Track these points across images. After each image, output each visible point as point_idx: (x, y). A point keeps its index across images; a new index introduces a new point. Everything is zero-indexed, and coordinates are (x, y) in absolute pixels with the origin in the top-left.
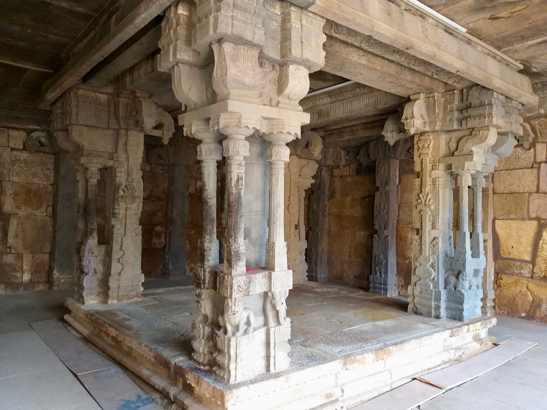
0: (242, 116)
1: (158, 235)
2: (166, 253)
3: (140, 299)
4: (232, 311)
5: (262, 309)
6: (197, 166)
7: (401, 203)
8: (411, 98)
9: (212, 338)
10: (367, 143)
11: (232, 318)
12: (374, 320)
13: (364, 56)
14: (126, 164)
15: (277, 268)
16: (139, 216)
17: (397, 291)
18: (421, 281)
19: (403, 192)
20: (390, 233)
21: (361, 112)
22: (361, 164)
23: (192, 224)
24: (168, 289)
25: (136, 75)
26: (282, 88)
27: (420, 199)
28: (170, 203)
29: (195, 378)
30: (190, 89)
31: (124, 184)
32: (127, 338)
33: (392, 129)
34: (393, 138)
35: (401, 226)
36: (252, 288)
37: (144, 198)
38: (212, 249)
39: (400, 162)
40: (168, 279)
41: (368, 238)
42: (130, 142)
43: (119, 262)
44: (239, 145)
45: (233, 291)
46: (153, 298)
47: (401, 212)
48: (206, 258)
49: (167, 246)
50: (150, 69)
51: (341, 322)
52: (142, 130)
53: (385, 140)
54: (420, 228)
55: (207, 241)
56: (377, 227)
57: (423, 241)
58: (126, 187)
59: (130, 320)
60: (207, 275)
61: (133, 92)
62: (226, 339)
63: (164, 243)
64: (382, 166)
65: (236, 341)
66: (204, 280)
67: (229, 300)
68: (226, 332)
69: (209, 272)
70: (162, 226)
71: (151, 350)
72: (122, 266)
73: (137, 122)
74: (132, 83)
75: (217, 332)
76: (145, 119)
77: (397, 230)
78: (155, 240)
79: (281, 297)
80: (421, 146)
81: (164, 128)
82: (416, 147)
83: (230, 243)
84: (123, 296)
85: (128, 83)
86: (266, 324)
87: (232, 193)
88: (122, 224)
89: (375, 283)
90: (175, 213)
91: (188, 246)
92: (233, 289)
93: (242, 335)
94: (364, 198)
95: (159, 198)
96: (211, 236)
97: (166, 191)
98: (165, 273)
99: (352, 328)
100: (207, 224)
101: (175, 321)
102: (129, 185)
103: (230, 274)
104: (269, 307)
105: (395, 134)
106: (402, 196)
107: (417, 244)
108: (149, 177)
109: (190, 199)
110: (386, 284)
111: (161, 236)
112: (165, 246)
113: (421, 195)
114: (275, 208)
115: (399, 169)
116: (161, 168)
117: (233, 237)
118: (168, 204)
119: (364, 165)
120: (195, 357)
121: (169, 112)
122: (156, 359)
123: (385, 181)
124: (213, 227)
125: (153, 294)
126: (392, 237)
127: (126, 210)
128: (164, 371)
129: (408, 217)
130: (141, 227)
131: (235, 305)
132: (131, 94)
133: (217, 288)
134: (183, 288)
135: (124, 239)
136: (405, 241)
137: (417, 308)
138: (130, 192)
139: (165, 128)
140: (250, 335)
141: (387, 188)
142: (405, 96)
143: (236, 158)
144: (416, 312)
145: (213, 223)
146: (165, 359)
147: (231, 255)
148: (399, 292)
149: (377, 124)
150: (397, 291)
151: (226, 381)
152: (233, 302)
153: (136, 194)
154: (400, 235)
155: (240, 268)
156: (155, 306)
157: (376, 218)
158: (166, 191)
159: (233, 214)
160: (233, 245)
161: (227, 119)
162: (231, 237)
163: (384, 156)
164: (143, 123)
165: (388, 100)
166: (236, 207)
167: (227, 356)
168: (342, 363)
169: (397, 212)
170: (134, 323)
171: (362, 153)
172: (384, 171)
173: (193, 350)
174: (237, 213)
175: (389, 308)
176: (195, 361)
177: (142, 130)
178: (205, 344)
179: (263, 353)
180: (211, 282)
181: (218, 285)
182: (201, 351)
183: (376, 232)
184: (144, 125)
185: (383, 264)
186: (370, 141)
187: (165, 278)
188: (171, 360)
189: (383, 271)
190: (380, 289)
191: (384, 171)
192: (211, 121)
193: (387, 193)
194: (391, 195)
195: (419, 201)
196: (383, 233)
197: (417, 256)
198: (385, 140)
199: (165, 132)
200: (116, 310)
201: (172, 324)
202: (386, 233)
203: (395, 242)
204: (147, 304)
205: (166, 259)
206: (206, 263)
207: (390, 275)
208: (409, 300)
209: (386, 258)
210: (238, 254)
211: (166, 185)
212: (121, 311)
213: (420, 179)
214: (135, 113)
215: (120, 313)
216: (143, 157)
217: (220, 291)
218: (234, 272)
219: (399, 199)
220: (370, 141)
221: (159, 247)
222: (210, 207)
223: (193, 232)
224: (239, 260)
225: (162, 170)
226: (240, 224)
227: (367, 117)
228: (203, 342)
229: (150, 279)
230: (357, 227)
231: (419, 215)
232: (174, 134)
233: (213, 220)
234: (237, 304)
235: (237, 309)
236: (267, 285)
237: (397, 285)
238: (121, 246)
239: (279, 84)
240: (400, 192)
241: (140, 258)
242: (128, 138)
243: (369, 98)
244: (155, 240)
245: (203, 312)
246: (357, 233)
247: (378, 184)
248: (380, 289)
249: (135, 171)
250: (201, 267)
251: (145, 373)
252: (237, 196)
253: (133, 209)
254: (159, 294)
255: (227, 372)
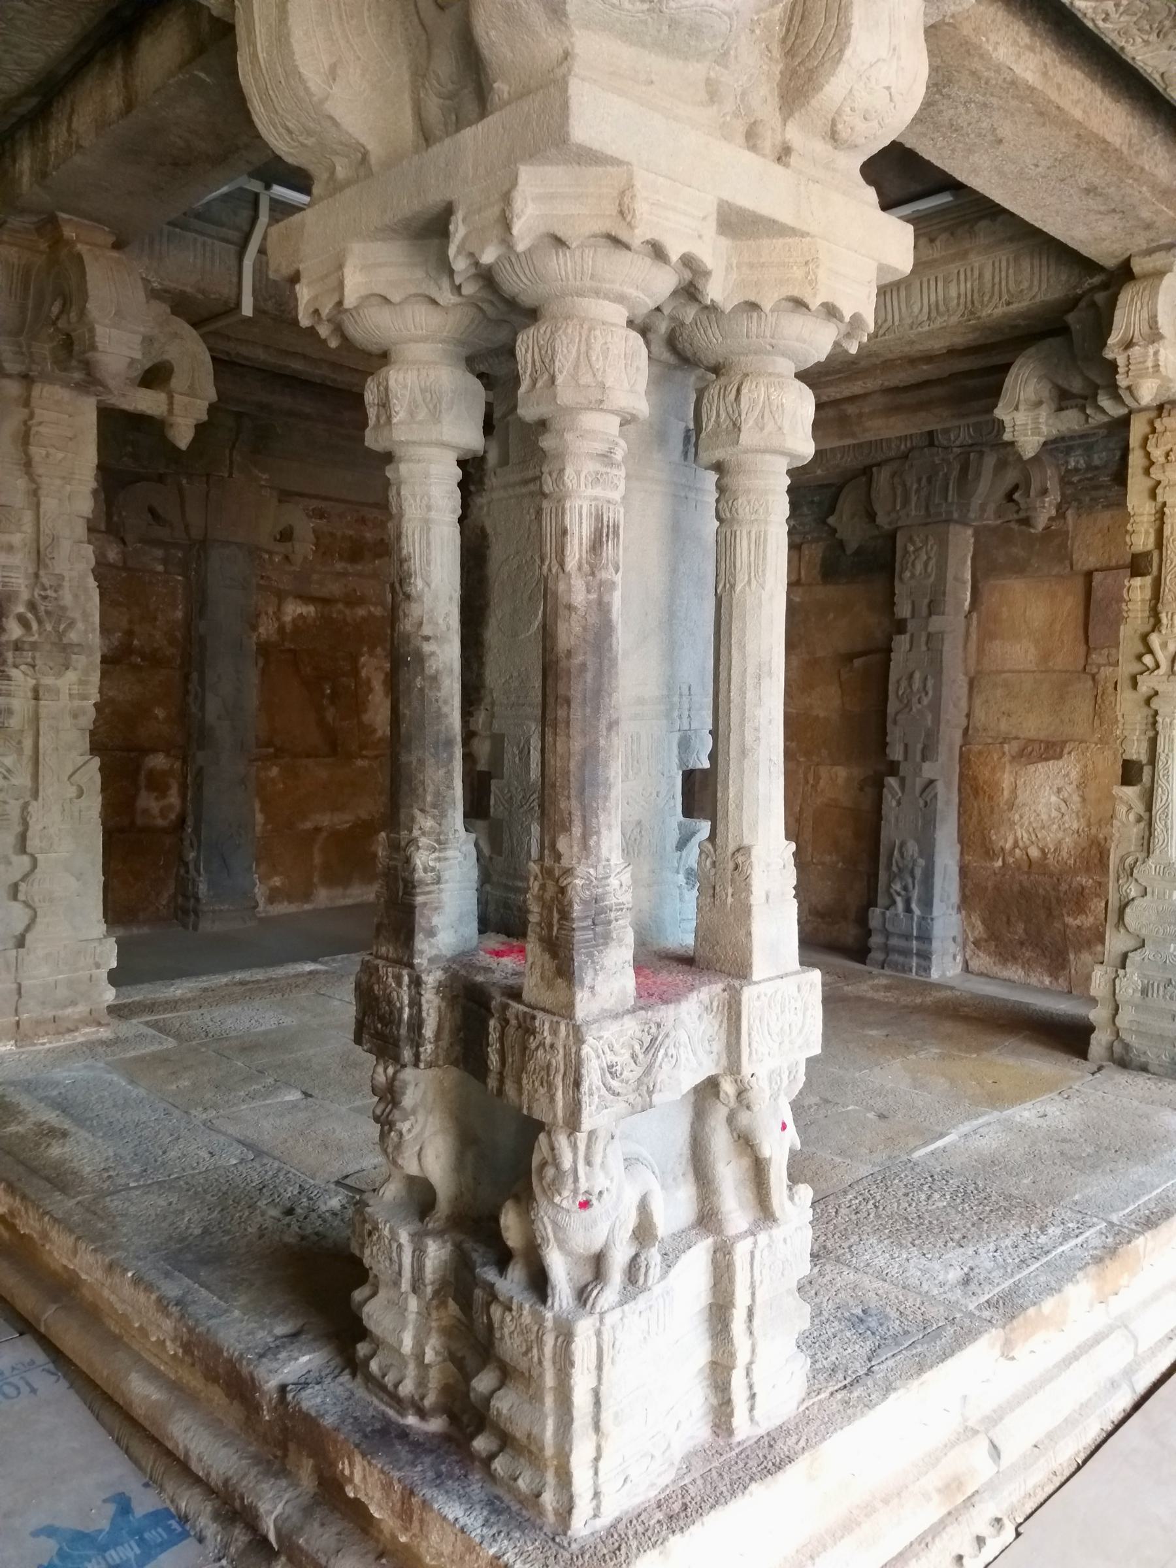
0: (638, 184)
1: (157, 784)
2: (187, 843)
3: (104, 1033)
4: (575, 1192)
5: (686, 1151)
6: (280, 548)
7: (978, 672)
8: (1137, 266)
9: (462, 1292)
10: (867, 471)
11: (575, 1221)
12: (996, 1100)
13: (1031, 49)
14: (28, 517)
15: (759, 969)
16: (89, 717)
17: (959, 958)
18: (1148, 951)
19: (987, 635)
20: (942, 770)
21: (912, 334)
22: (841, 545)
23: (269, 744)
24: (205, 982)
25: (57, 138)
26: (811, 71)
27: (1150, 651)
28: (195, 676)
29: (387, 1487)
30: (333, 69)
31: (25, 595)
32: (54, 1234)
33: (1033, 397)
34: (1036, 431)
35: (976, 748)
36: (663, 1074)
37: (104, 660)
38: (446, 875)
39: (976, 534)
40: (195, 928)
41: (861, 789)
42: (41, 429)
43: (15, 897)
44: (606, 352)
45: (585, 1099)
46: (154, 1025)
47: (978, 702)
48: (420, 921)
49: (190, 821)
50: (116, 103)
51: (882, 1116)
52: (90, 380)
53: (1007, 437)
54: (1144, 758)
55: (423, 841)
56: (896, 753)
57: (1158, 806)
58: (32, 606)
59: (65, 1134)
60: (431, 1002)
61: (49, 225)
62: (549, 1324)
63: (178, 809)
64: (917, 550)
65: (599, 1334)
66: (417, 1024)
67: (562, 1141)
68: (539, 1283)
69: (440, 988)
70: (168, 755)
71: (162, 1305)
72: (29, 912)
73: (68, 343)
74: (41, 175)
75: (489, 1274)
76: (99, 330)
77: (964, 760)
78: (147, 802)
79: (775, 1097)
80: (1157, 454)
81: (174, 383)
82: (1136, 460)
83: (558, 857)
84: (38, 1023)
85: (25, 180)
86: (707, 1218)
87: (569, 607)
88: (20, 751)
89: (887, 935)
90: (213, 707)
91: (260, 818)
92: (585, 1087)
93: (622, 1303)
94: (850, 657)
95: (154, 660)
96: (443, 815)
97: (178, 634)
98: (185, 910)
99: (940, 1143)
100: (421, 762)
101: (251, 1134)
102: (45, 598)
103: (567, 1010)
104: (720, 1141)
105: (1044, 413)
106: (981, 651)
107: (1132, 817)
108: (118, 585)
109: (261, 663)
110: (925, 937)
111: (168, 787)
112: (182, 821)
113: (1155, 640)
114: (750, 682)
115: (974, 559)
116: (159, 553)
117: (577, 831)
118: (186, 678)
119: (852, 546)
120: (374, 1366)
121: (195, 325)
122: (187, 1347)
123: (926, 601)
124: (449, 773)
125: (151, 1007)
126: (948, 785)
127: (37, 698)
128: (233, 1413)
129: (1004, 720)
130: (96, 762)
131: (589, 1163)
132: (39, 229)
133: (486, 1069)
134: (259, 975)
135: (34, 807)
136: (991, 798)
137: (1127, 1047)
138: (49, 627)
139: (178, 382)
140: (657, 1290)
141: (936, 624)
142: (1102, 262)
143: (591, 420)
144: (1124, 1060)
145: (451, 758)
146: (230, 1361)
147: (565, 915)
148: (966, 963)
149: (937, 391)
150: (959, 958)
151: (551, 1518)
152: (582, 1146)
153: (73, 636)
154: (975, 778)
155: (608, 979)
156: (161, 1059)
157: (895, 722)
158: (178, 634)
159: (576, 713)
160: (581, 870)
161: (552, 197)
162: (566, 828)
163: (928, 514)
164: (93, 347)
165: (1025, 285)
166: (589, 676)
167: (549, 1401)
168: (998, 1345)
169: (964, 704)
170: (82, 1152)
171: (847, 505)
172: (926, 564)
173: (363, 1333)
174: (597, 710)
175: (1012, 1042)
176: (376, 1384)
177: (90, 380)
178: (425, 1313)
179: (700, 1352)
180: (446, 1035)
181: (494, 1059)
182: (407, 1344)
183: (893, 768)
184: (98, 356)
185: (918, 872)
186: (879, 465)
187: (185, 926)
188: (261, 1372)
189: (915, 895)
190: (906, 953)
191: (926, 564)
192: (459, 216)
193: (934, 641)
194: (947, 647)
195: (1148, 659)
196: (918, 771)
197: (1130, 860)
198: (1007, 437)
199: (177, 397)
200: (12, 1083)
201: (239, 1150)
202: (929, 770)
203: (957, 800)
204: (133, 1053)
205: (186, 864)
206: (421, 943)
207: (938, 909)
208: (1098, 1015)
209: (928, 852)
210: (603, 911)
211: (179, 614)
212: (28, 1086)
213: (1148, 580)
214: (55, 310)
215: (24, 1101)
216: (95, 493)
217: (510, 1089)
218: (585, 1005)
219: (972, 662)
220: (879, 465)
221: (160, 822)
222: (434, 678)
223: (274, 771)
224: (606, 938)
225: (165, 561)
226: (607, 766)
227: (929, 358)
228: (413, 1304)
229: (135, 931)
230: (824, 752)
231: (1146, 711)
232: (212, 409)
233: (449, 743)
234: (597, 1159)
235: (600, 1181)
236: (718, 1046)
237: (959, 940)
238: (23, 838)
239: (790, 53)
240: (974, 636)
241: (96, 879)
242: (32, 416)
243: (947, 282)
244: (147, 802)
245: (413, 1169)
246: (824, 771)
247: (903, 610)
248: (906, 953)
249: (66, 546)
250: (398, 962)
251: (141, 1391)
252: (593, 619)
253: (64, 696)
254: (173, 1005)
255: (550, 1477)
